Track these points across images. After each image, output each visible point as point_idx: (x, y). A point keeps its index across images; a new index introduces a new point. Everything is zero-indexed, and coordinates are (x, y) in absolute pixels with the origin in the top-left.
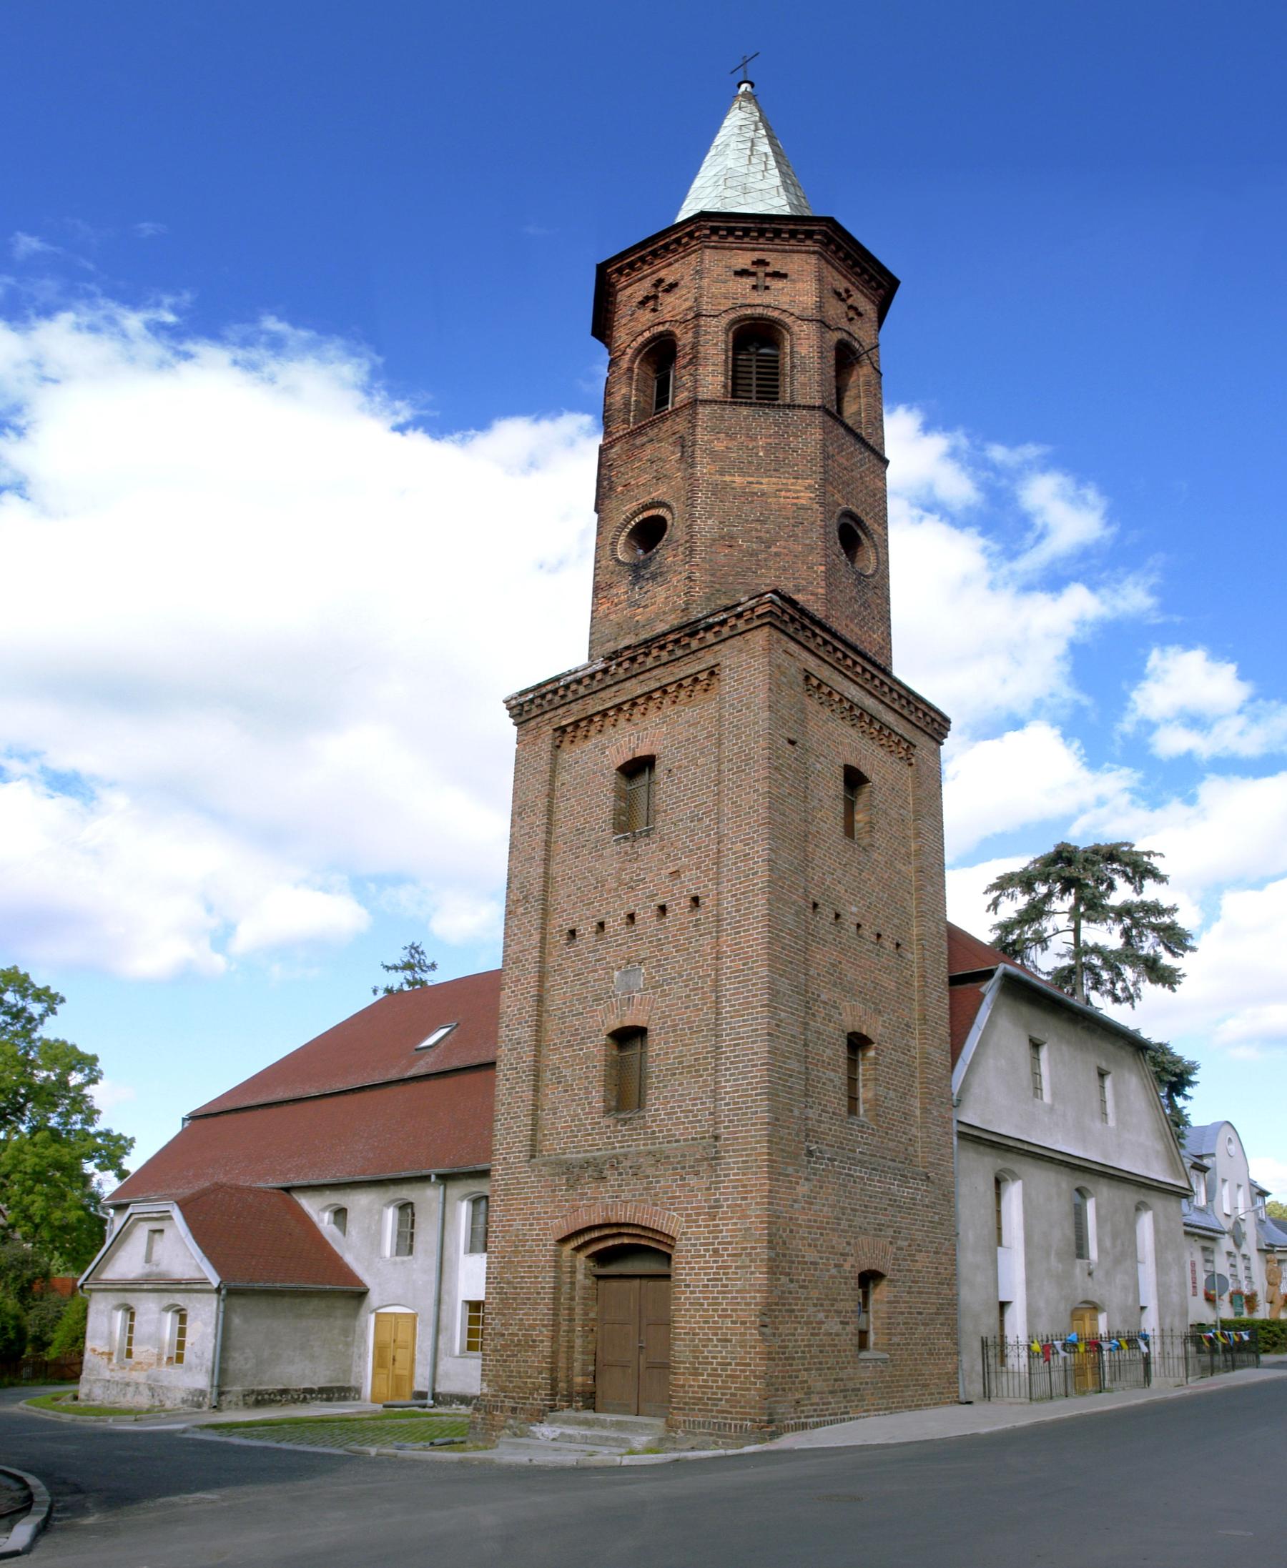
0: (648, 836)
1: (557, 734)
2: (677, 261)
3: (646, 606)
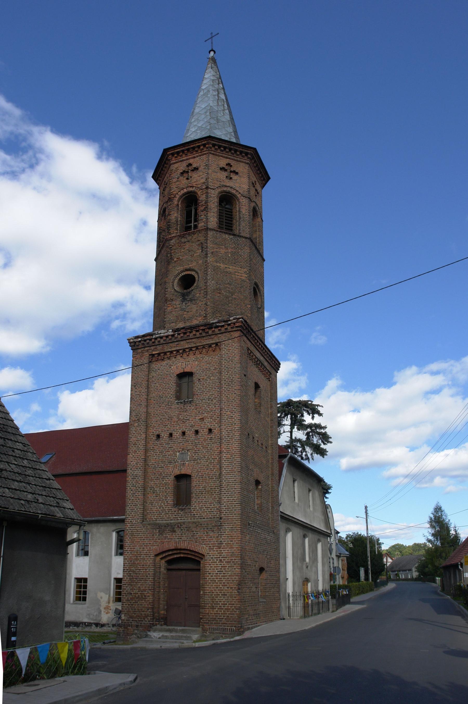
0: (190, 403)
1: (150, 357)
2: (197, 156)
3: (188, 312)
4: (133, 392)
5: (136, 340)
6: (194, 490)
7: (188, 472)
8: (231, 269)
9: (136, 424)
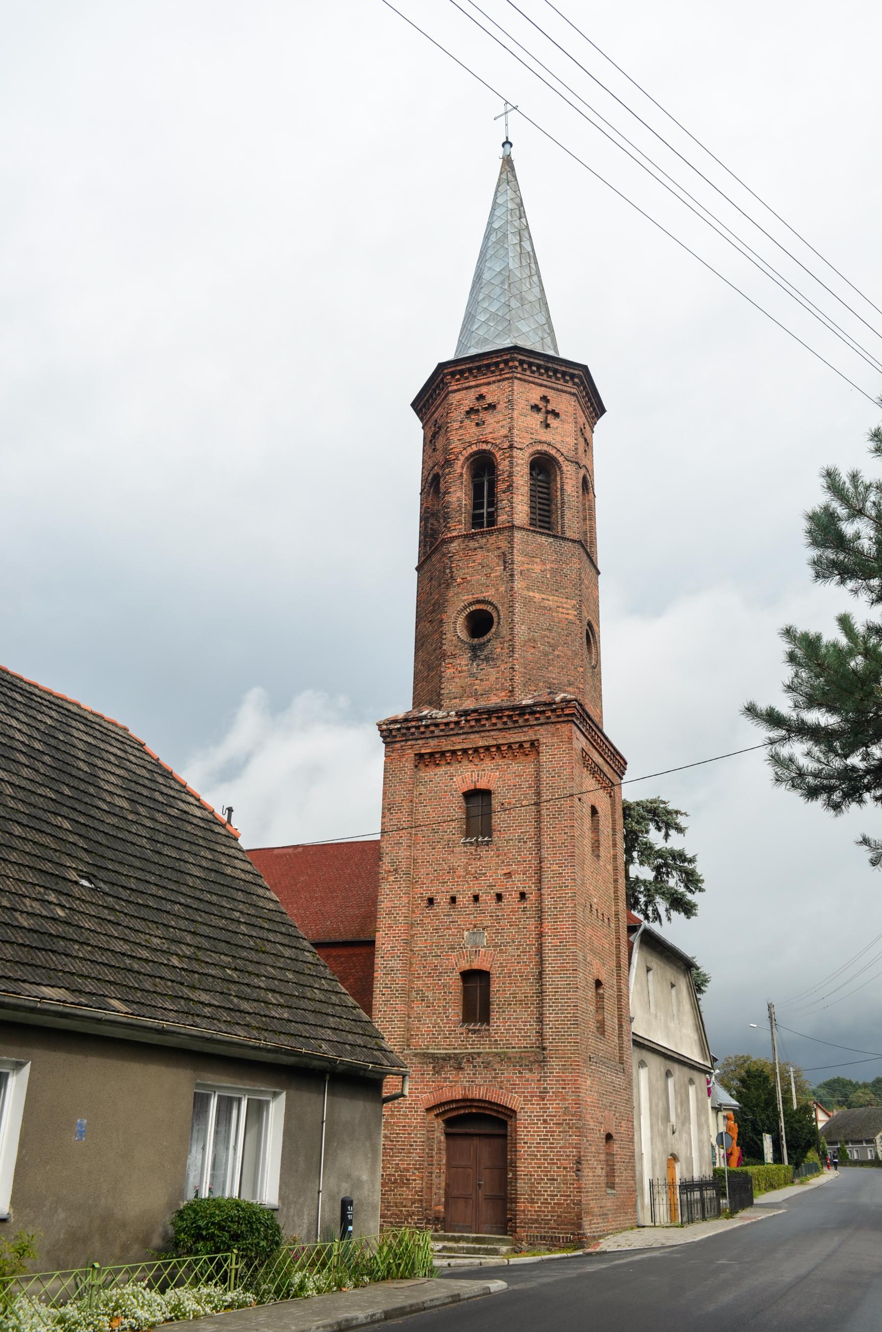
0: (487, 845)
2: (494, 382)
4: (385, 820)
5: (392, 727)
6: (495, 998)
7: (485, 966)
8: (552, 601)
9: (392, 878)
